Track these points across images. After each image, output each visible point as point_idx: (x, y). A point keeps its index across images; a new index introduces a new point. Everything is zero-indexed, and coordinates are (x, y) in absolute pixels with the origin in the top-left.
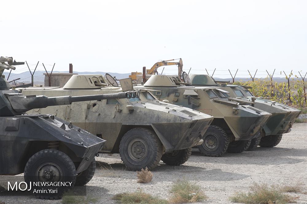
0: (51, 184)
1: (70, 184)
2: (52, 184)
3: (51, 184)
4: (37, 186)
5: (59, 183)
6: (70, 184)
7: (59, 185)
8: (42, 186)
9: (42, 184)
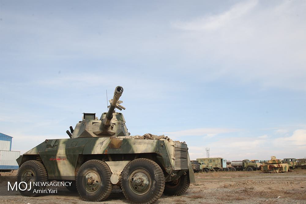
0: (51, 184)
1: (70, 184)
2: (52, 184)
3: (51, 184)
4: (37, 186)
5: (59, 183)
6: (70, 184)
7: (59, 185)
8: (42, 186)
9: (43, 184)
